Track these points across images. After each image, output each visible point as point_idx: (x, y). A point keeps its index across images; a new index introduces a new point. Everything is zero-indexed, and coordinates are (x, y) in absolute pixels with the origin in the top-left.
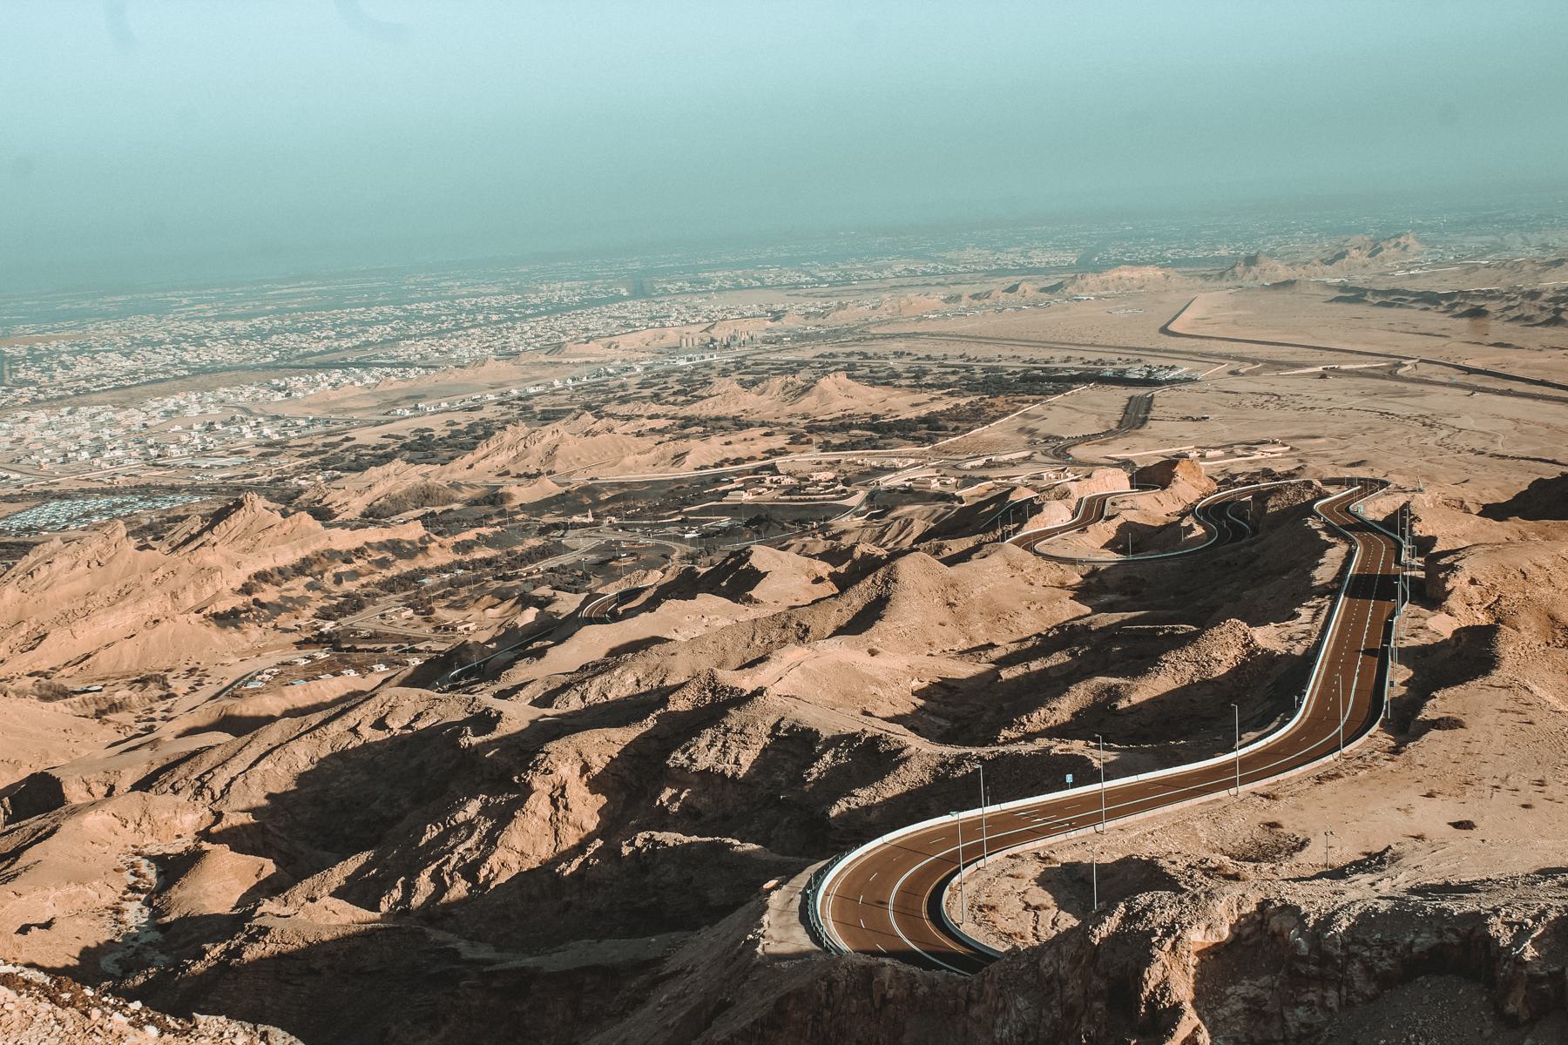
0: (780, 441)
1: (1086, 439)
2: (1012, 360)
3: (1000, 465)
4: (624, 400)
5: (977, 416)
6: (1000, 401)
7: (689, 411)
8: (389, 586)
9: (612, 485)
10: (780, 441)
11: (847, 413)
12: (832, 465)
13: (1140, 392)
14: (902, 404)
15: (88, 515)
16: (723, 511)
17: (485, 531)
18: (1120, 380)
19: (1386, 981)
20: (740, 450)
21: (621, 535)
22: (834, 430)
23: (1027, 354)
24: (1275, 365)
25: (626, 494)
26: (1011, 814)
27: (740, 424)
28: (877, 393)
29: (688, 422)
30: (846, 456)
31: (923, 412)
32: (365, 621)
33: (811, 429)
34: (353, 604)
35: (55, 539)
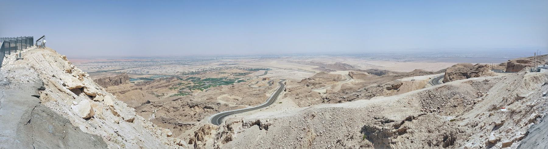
0: (229, 75)
1: (261, 76)
2: (254, 68)
3: (251, 78)
4: (214, 70)
5: (249, 73)
6: (252, 72)
7: (220, 71)
8: (187, 87)
9: (211, 78)
10: (229, 75)
11: (470, 65)
12: (234, 77)
13: (266, 71)
14: (242, 72)
15: (159, 77)
16: (223, 82)
17: (198, 82)
18: (264, 70)
19: (251, 126)
20: (225, 75)
21: (211, 83)
22: (235, 74)
23: (255, 67)
24: (280, 68)
25: (213, 79)
26: (233, 111)
27: (225, 73)
28: (240, 70)
29: (220, 72)
30: (237, 77)
31: (244, 73)
32: (185, 90)
33: (232, 74)
34: (183, 89)
35: (221, 127)
